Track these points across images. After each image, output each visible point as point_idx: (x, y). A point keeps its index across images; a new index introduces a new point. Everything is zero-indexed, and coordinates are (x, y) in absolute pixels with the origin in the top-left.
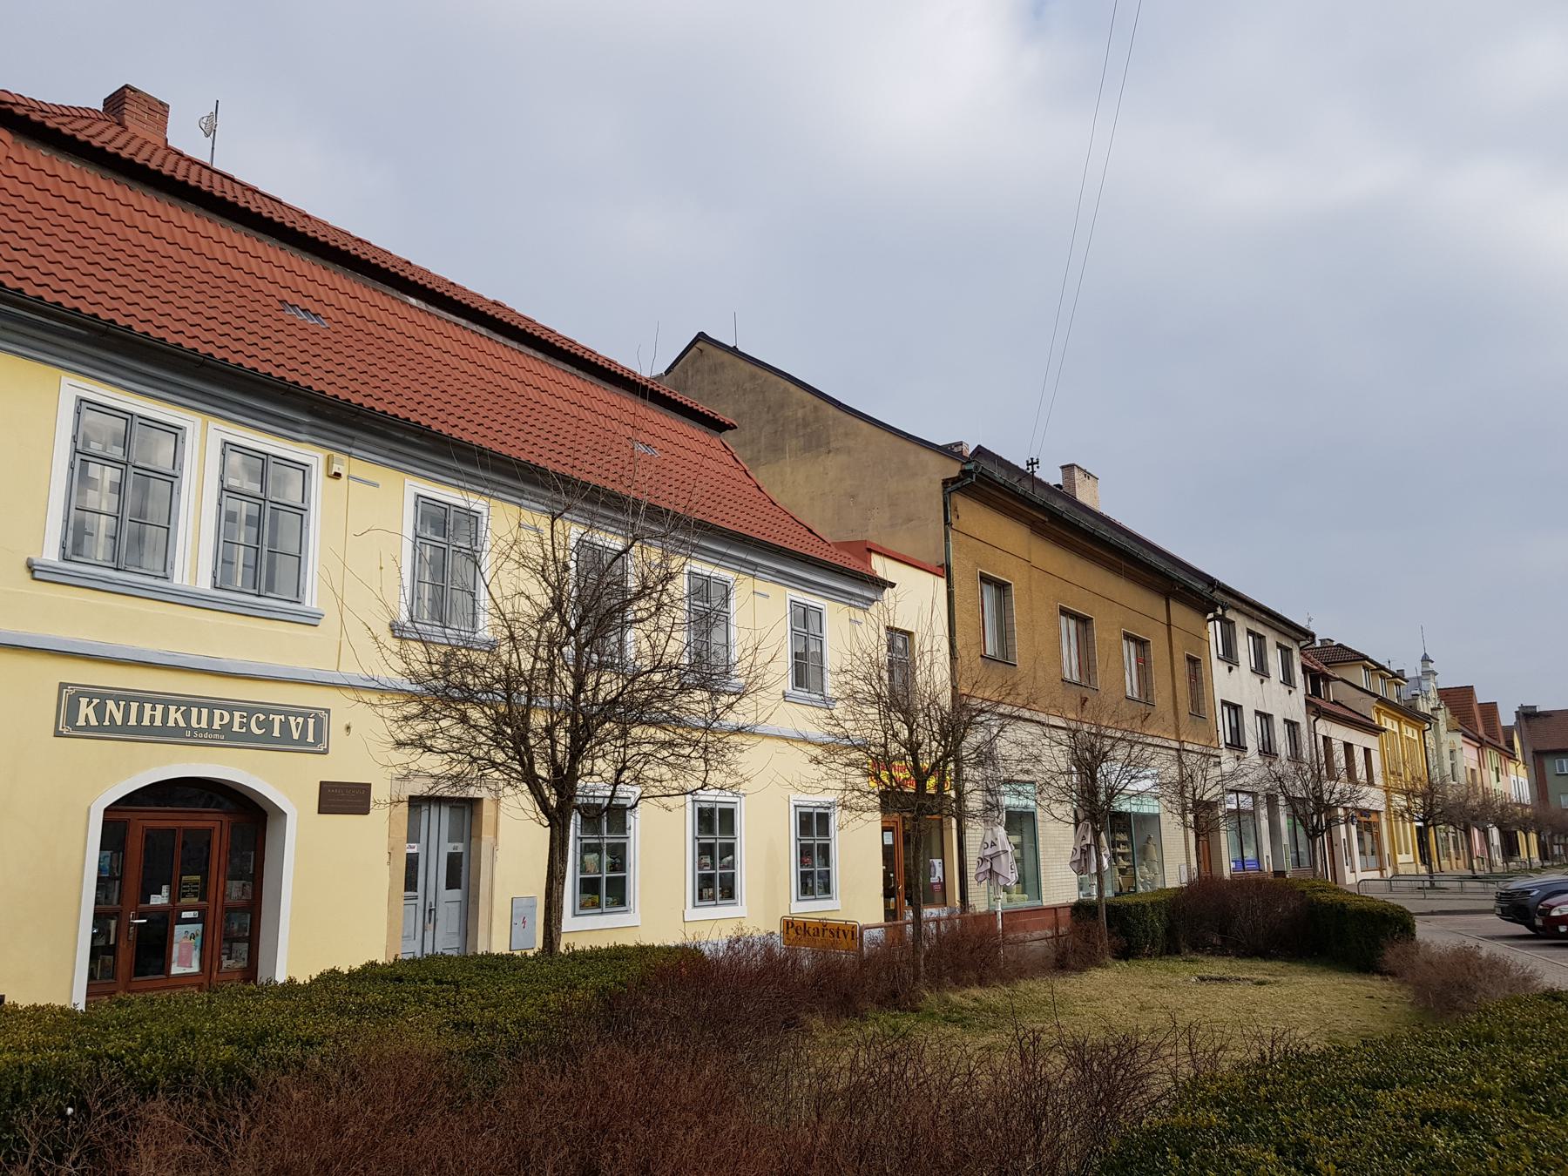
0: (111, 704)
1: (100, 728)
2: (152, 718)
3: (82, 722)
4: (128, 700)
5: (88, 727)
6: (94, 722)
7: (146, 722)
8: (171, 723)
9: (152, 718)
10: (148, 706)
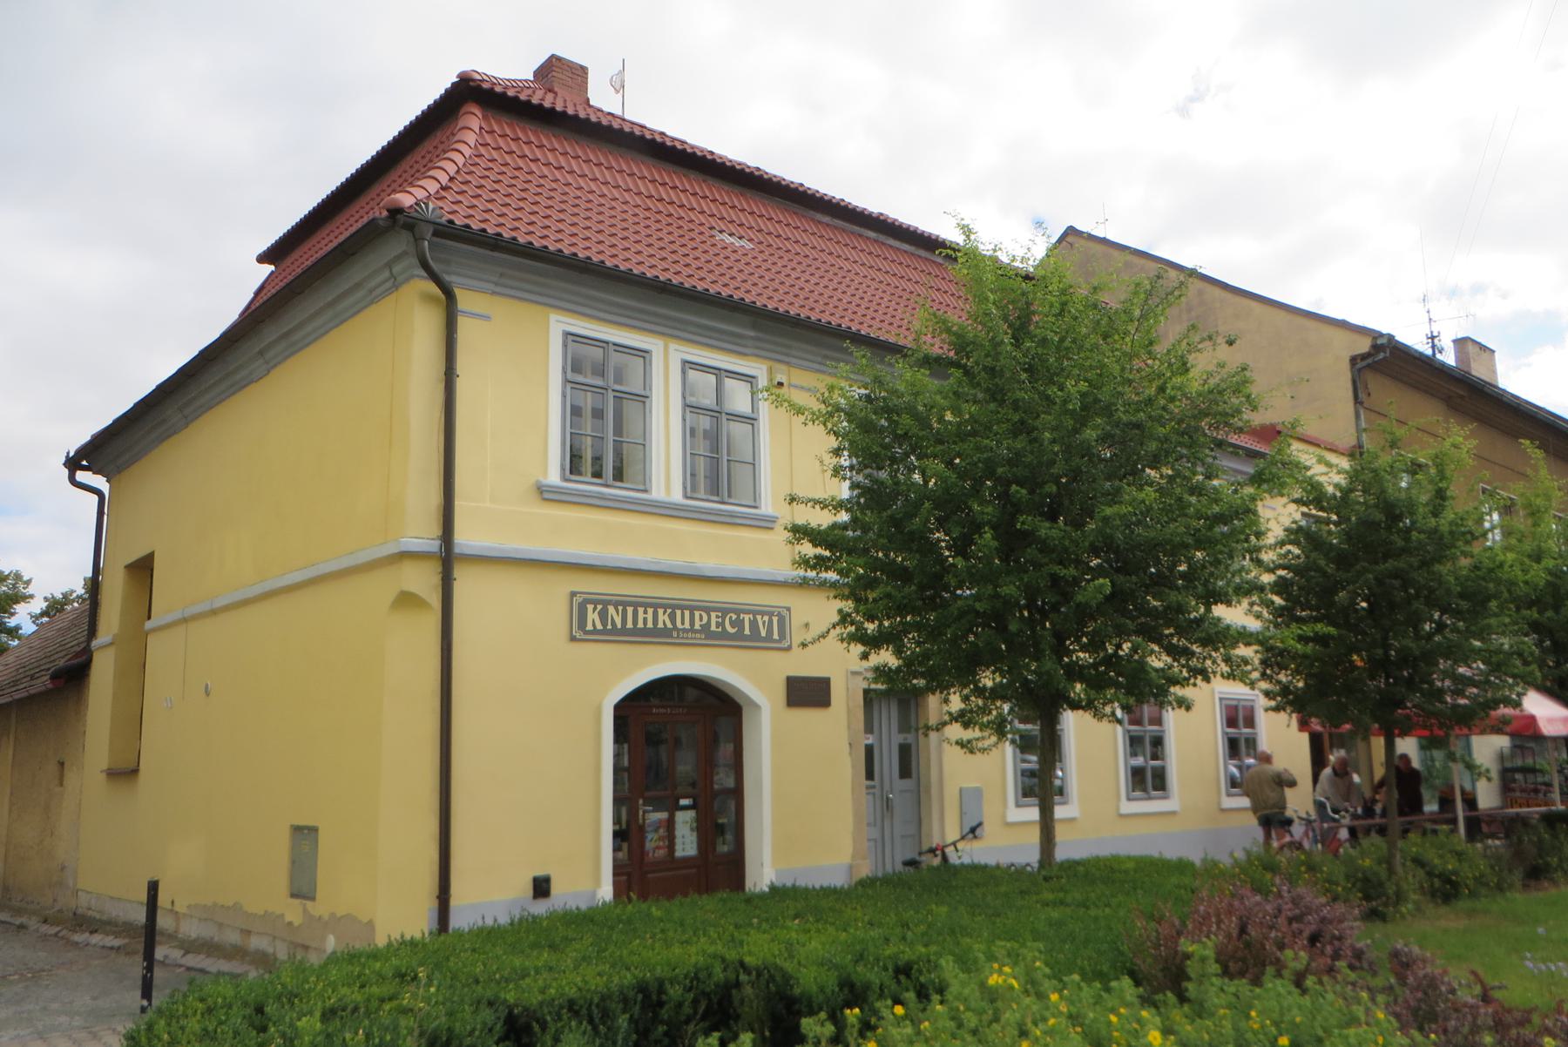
0: (611, 610)
1: (604, 632)
2: (645, 620)
3: (589, 627)
4: (625, 604)
5: (595, 631)
6: (599, 626)
7: (640, 625)
8: (660, 625)
9: (645, 620)
10: (641, 610)
